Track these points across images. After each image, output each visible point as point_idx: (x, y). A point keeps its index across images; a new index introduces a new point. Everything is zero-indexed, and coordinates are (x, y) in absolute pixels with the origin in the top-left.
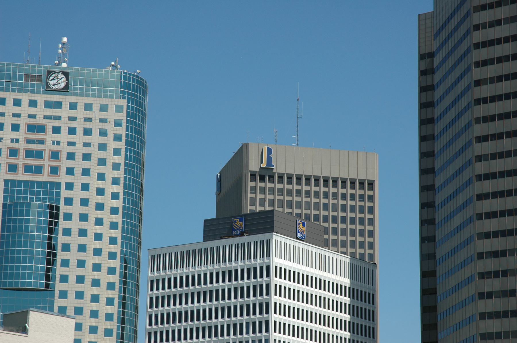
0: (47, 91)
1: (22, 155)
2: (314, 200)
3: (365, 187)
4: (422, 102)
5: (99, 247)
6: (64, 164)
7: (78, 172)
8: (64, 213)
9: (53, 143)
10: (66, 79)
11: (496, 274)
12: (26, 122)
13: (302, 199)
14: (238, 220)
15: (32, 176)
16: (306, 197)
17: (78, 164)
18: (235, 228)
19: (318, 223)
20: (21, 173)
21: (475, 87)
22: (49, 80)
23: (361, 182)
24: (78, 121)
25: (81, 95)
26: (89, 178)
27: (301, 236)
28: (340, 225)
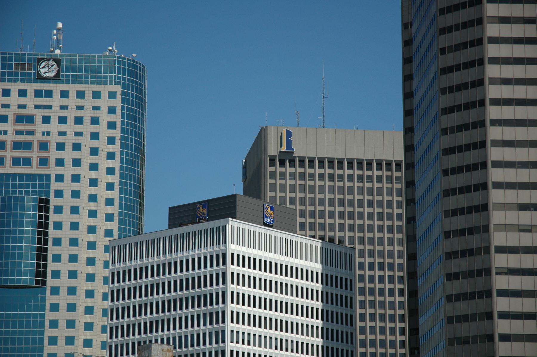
0: (37, 80)
1: (10, 147)
2: (348, 184)
3: (276, 163)
4: (406, 74)
5: (93, 241)
6: (53, 154)
7: (68, 162)
8: (55, 206)
9: (43, 134)
10: (57, 66)
11: (463, 254)
12: (15, 113)
13: (325, 183)
14: (202, 207)
15: (20, 169)
16: (329, 181)
17: (68, 155)
18: (199, 215)
19: (284, 206)
20: (9, 166)
21: (440, 55)
22: (39, 67)
23: (272, 158)
24: (54, 109)
25: (74, 82)
26: (63, 168)
27: (269, 221)
28: (356, 208)
